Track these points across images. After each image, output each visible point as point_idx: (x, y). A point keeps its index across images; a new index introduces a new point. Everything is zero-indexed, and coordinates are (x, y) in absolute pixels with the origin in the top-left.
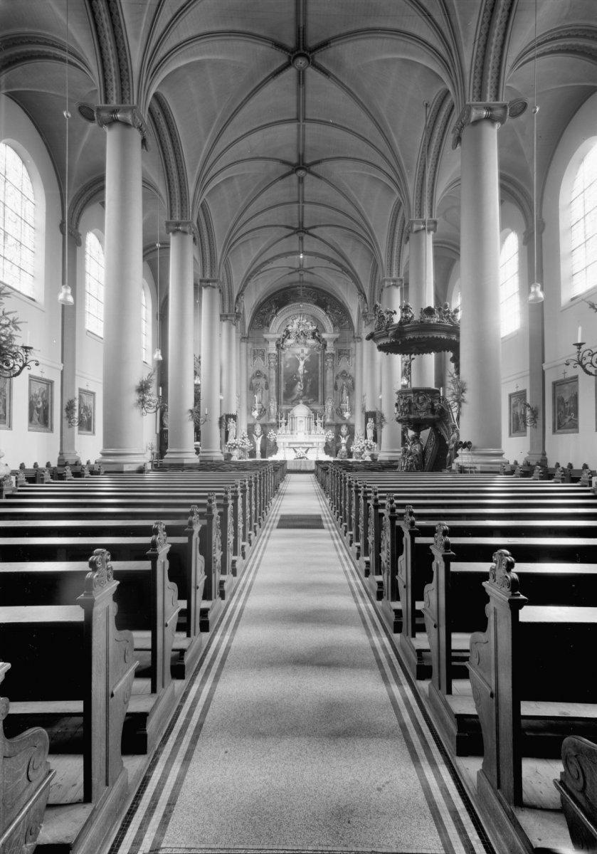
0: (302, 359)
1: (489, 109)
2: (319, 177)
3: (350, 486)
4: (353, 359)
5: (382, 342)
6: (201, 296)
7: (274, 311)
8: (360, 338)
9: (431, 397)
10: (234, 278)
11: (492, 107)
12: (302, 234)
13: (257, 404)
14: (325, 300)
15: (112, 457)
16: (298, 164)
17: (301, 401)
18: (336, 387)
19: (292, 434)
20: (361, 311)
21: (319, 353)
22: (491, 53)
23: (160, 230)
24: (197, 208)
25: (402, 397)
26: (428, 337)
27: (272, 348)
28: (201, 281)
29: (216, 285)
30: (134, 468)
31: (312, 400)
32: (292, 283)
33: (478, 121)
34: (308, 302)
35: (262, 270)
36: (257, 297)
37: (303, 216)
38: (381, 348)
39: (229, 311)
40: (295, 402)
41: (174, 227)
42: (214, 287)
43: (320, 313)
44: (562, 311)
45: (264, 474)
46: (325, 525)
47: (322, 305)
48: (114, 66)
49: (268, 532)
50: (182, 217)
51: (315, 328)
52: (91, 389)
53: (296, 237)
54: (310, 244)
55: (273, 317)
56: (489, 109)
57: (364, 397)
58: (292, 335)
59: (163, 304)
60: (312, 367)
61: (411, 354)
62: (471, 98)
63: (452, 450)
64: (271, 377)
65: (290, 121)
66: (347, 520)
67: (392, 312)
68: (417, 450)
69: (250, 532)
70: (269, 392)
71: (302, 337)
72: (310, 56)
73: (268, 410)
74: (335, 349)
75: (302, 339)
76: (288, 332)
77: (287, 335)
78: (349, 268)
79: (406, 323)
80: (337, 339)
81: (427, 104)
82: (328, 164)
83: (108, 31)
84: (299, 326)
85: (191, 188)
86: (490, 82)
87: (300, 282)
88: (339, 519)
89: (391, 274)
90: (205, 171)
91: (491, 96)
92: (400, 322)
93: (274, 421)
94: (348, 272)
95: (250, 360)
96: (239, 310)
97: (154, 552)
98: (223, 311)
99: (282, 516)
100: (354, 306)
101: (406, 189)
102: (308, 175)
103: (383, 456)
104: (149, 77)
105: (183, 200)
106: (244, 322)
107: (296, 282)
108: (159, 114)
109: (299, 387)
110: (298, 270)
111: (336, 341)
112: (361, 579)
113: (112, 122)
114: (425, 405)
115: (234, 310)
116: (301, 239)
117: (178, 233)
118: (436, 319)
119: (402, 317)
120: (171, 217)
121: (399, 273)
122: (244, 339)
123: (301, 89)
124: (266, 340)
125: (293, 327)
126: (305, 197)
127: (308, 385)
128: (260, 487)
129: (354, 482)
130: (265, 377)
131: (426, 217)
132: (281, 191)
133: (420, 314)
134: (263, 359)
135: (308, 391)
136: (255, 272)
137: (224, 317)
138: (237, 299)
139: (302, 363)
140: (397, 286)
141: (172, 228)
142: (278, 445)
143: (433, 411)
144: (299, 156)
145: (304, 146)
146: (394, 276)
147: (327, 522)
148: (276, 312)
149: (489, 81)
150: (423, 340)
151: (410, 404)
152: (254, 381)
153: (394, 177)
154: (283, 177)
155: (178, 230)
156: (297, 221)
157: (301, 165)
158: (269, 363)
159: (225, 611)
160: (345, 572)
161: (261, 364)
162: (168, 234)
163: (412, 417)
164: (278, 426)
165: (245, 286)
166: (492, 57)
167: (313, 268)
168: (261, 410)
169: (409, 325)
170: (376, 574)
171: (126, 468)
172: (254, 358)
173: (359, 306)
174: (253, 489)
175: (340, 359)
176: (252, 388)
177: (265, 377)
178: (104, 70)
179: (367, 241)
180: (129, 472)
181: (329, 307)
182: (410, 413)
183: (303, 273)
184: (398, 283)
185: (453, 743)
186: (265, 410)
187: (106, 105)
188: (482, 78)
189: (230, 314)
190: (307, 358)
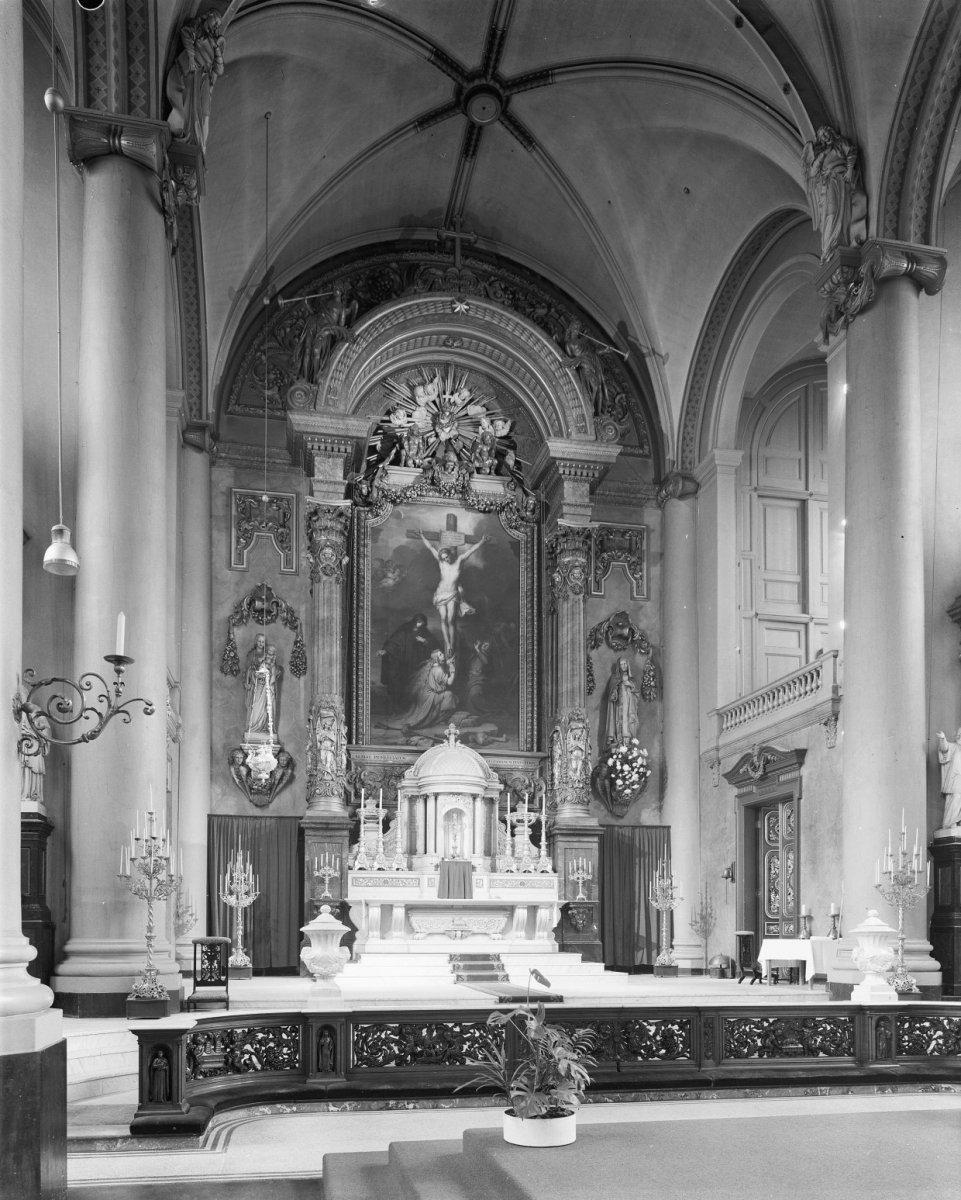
7: (339, 313)
19: (410, 867)
31: (490, 727)
40: (430, 732)
51: (502, 429)
55: (334, 342)
70: (312, 688)
93: (332, 807)
109: (438, 671)
127: (476, 670)
130: (292, 622)
135: (474, 691)
138: (178, 46)
139: (450, 572)
148: (350, 322)
152: (239, 633)
164: (354, 837)
172: (246, 535)
177: (292, 622)
190: (468, 551)
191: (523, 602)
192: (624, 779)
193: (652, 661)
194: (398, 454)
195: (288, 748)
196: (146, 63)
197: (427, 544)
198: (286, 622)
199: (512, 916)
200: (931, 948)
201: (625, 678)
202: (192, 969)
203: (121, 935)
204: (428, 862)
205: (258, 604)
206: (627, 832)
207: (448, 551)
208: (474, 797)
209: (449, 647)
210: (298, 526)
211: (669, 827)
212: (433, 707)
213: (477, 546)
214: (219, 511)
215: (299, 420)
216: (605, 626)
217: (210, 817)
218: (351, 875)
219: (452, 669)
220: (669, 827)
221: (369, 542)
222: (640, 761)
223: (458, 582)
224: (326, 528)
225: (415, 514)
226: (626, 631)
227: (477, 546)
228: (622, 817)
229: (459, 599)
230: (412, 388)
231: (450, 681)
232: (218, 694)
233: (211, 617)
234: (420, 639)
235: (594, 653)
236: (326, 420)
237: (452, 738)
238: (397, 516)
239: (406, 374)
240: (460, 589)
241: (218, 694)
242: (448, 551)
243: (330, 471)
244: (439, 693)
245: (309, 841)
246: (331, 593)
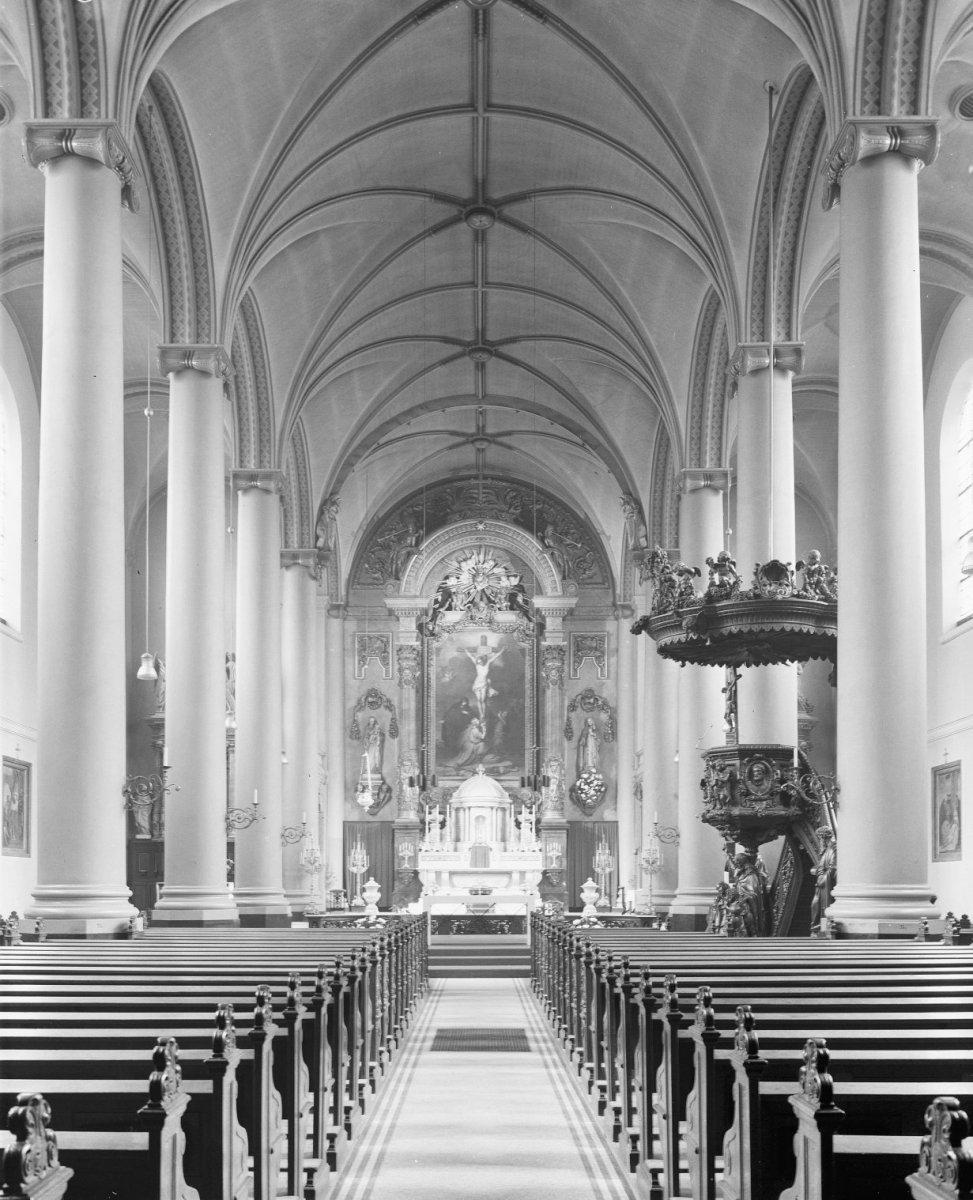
0: (484, 660)
1: (897, 132)
2: (523, 229)
3: (578, 957)
4: (613, 660)
5: (668, 638)
6: (236, 506)
7: (411, 540)
8: (628, 607)
9: (782, 767)
10: (313, 462)
11: (905, 127)
12: (484, 356)
13: (369, 775)
14: (546, 514)
15: (58, 903)
16: (474, 200)
17: (481, 768)
18: (568, 732)
19: (456, 850)
20: (631, 543)
21: (526, 645)
22: (898, 12)
23: (153, 362)
24: (234, 318)
25: (714, 767)
26: (772, 630)
27: (406, 633)
28: (236, 476)
29: (272, 486)
30: (109, 927)
31: (508, 763)
32: (455, 470)
33: (874, 158)
34: (497, 518)
35: (383, 440)
36: (370, 503)
37: (484, 318)
38: (666, 652)
39: (302, 544)
40: (467, 769)
41: (177, 360)
42: (267, 491)
43: (529, 545)
44: (944, 643)
45: (389, 944)
46: (532, 1045)
47: (526, 522)
48: (66, 37)
49: (413, 1057)
50: (198, 335)
51: (515, 581)
53: (468, 363)
54: (503, 380)
55: (409, 555)
56: (897, 132)
57: (639, 756)
58: (457, 601)
59: (135, 524)
60: (506, 678)
62: (858, 107)
63: (822, 887)
64: (405, 706)
65: (462, 285)
66: (584, 1042)
67: (689, 572)
68: (750, 888)
69: (361, 1081)
70: (400, 743)
71: (482, 605)
72: (496, 211)
74: (568, 635)
75: (483, 611)
76: (447, 594)
77: (444, 601)
78: (601, 439)
80: (571, 612)
81: (771, 89)
82: (543, 201)
83: (183, 234)
84: (474, 577)
85: (220, 269)
86: (898, 73)
87: (477, 467)
88: (595, 1089)
89: (700, 462)
91: (902, 103)
92: (708, 595)
93: (412, 816)
94: (596, 446)
95: (353, 663)
96: (326, 541)
97: (219, 1059)
98: (286, 544)
99: (439, 1031)
100: (614, 530)
101: (729, 269)
102: (498, 225)
103: (683, 905)
104: (142, 46)
105: (200, 297)
106: (336, 572)
107: (468, 467)
108: (150, 108)
109: (475, 731)
110: (471, 439)
111: (569, 615)
112: (591, 1118)
113: (60, 156)
114: (767, 785)
115: (312, 542)
116: (481, 367)
117: (189, 375)
118: (789, 590)
119: (712, 584)
120: (173, 335)
121: (719, 459)
122: (337, 609)
123: (481, 45)
124: (391, 612)
125: (462, 582)
126: (496, 88)
127: (498, 729)
128: (390, 969)
129: (584, 948)
130: (390, 707)
131: (775, 336)
132: (436, 259)
133: (753, 578)
134: (385, 660)
135: (498, 741)
136: (364, 445)
137: (289, 559)
138: (321, 512)
139: (482, 671)
140: (716, 490)
141: (45, 143)
142: (421, 877)
143: (785, 799)
144: (475, 181)
145: (486, 161)
146: (709, 466)
147: (536, 1040)
148: (418, 544)
149: (709, 431)
150: (762, 636)
151: (733, 782)
152: (360, 716)
153: (701, 240)
154: (437, 229)
155: (189, 368)
156: (470, 327)
157: (481, 204)
158: (400, 670)
160: (572, 1130)
161: (384, 677)
162: (165, 374)
163: (736, 811)
164: (423, 831)
165: (340, 481)
166: (901, 21)
167: (509, 433)
168: (380, 788)
170: (599, 1079)
171: (92, 928)
172: (363, 659)
173: (626, 533)
175: (578, 660)
176: (356, 734)
177: (390, 707)
178: (43, 44)
179: (643, 379)
180: (96, 936)
181: (550, 530)
182: (734, 803)
183: (485, 445)
184: (718, 482)
185: (625, 1163)
186: (389, 790)
187: (47, 121)
188: (881, 63)
189: (308, 554)
190: (494, 658)
191: (528, 686)
192: (586, 794)
193: (610, 718)
194: (450, 605)
195: (388, 781)
196: (308, 525)
197: (469, 655)
198: (387, 707)
199: (511, 877)
200: (130, 893)
201: (590, 730)
203: (300, 888)
204: (465, 846)
205: (370, 699)
206: (590, 825)
207: (481, 658)
208: (492, 808)
209: (482, 716)
210: (392, 656)
211: (617, 822)
212: (473, 752)
213: (498, 654)
214: (348, 646)
215: (390, 602)
216: (580, 697)
217: (344, 822)
218: (420, 855)
219: (484, 729)
220: (617, 822)
221: (434, 657)
222: (595, 782)
223: (488, 676)
224: (406, 658)
225: (461, 638)
226: (592, 700)
227: (498, 654)
228: (591, 815)
229: (488, 686)
230: (459, 563)
231: (483, 736)
232: (349, 751)
233: (344, 708)
234: (465, 712)
235: (573, 715)
236: (404, 601)
237: (481, 773)
238: (451, 639)
239: (456, 555)
240: (489, 681)
241: (349, 751)
242: (481, 658)
243: (409, 625)
244: (476, 744)
245: (397, 836)
246: (410, 694)
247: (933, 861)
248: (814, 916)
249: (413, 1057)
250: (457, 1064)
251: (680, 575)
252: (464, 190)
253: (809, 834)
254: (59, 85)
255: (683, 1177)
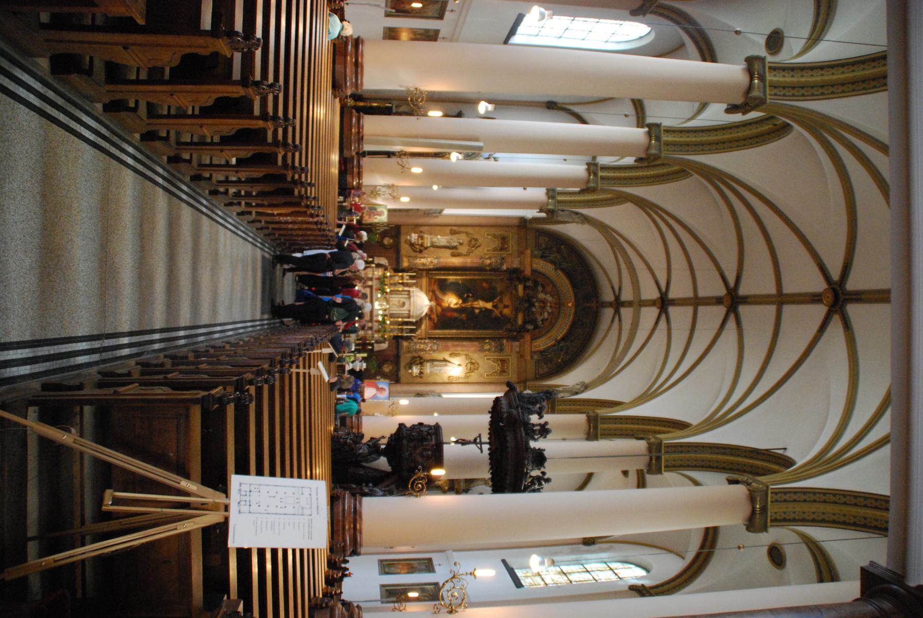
49: (259, 245)
52: (447, 15)
61: (489, 443)
73: (419, 255)
79: (526, 431)
90: (732, 183)
93: (405, 264)
110: (617, 298)
113: (750, 71)
127: (455, 315)
138: (577, 213)
148: (563, 270)
159: (200, 195)
163: (405, 442)
169: (523, 434)
174: (311, 226)
190: (497, 312)
202: (367, 148)
211: (766, 531)
220: (766, 531)
223: (486, 309)
229: (480, 309)
231: (452, 306)
247: (381, 561)
248: (345, 485)
249: (259, 245)
250: (254, 270)
251: (540, 408)
252: (742, 291)
253: (392, 484)
254: (784, 76)
255: (215, 162)
